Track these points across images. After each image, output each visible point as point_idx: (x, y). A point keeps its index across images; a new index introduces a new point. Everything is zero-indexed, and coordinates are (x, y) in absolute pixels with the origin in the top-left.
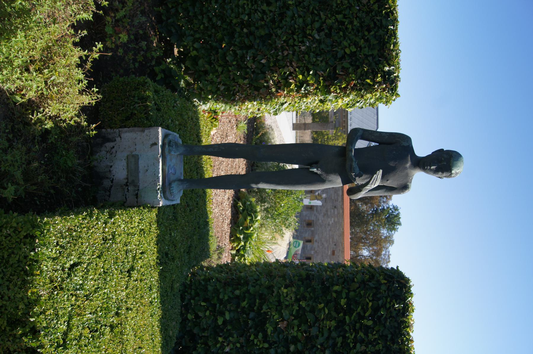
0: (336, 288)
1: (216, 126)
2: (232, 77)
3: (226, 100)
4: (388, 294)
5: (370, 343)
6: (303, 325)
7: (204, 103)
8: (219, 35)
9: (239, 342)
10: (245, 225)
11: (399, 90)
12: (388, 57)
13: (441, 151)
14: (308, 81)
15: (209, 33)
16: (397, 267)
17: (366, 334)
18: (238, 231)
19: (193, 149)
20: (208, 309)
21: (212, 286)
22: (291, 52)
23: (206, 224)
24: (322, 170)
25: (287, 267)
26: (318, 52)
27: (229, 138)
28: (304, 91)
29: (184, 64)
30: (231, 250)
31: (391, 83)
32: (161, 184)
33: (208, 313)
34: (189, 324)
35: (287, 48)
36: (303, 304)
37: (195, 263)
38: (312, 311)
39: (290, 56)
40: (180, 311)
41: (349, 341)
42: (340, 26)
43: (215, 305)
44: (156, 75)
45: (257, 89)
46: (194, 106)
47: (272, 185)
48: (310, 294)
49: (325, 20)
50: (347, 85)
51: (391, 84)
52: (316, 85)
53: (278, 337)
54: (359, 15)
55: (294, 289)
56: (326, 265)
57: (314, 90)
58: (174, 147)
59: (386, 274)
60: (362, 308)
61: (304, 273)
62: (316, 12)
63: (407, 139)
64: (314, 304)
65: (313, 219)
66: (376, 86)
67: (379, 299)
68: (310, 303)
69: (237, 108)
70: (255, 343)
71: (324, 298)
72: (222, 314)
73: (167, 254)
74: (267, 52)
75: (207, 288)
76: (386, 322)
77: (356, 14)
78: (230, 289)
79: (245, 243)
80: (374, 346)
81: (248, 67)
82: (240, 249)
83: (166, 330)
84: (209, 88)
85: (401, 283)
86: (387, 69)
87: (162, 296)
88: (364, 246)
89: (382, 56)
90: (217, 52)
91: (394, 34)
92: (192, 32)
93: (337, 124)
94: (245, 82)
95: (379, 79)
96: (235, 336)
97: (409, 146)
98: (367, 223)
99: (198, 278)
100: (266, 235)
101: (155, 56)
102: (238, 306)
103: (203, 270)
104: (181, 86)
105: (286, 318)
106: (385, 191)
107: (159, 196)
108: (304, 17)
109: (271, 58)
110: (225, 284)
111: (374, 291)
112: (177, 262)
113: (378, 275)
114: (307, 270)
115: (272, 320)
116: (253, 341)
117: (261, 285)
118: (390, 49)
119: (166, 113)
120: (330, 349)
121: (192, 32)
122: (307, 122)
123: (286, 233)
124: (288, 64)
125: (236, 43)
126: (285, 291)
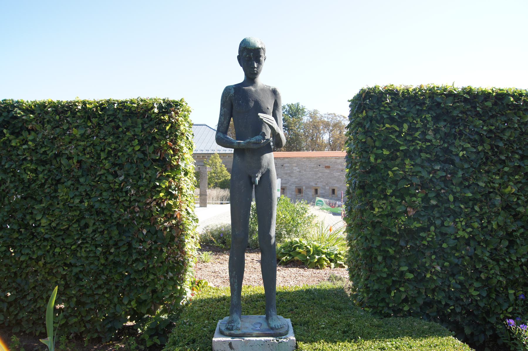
0: (372, 159)
1: (206, 283)
2: (160, 264)
3: (183, 270)
4: (376, 109)
5: (425, 126)
6: (410, 192)
7: (185, 294)
8: (116, 277)
9: (430, 256)
10: (305, 253)
11: (177, 99)
12: (145, 109)
13: (239, 58)
14: (166, 187)
15: (113, 287)
16: (349, 101)
17: (417, 130)
18: (311, 261)
19: (235, 304)
20: (397, 289)
21: (374, 285)
22: (136, 204)
23: (308, 291)
24: (258, 172)
25: (351, 208)
26: (137, 177)
27: (217, 270)
28: (176, 191)
29: (144, 315)
30: (330, 268)
31: (170, 107)
32: (272, 338)
33: (402, 289)
34: (414, 308)
35: (132, 208)
36: (389, 192)
37: (350, 303)
38: (396, 182)
39: (141, 204)
40: (402, 318)
41: (424, 146)
42: (112, 155)
43: (393, 281)
44: (155, 344)
45: (172, 238)
46: (187, 304)
47: (272, 223)
48: (379, 185)
49: (105, 169)
50: (171, 148)
51: (171, 106)
52: (171, 179)
53: (424, 216)
54: (102, 136)
55: (375, 201)
56: (348, 170)
57: (174, 181)
58: (233, 324)
59: (357, 112)
60: (391, 133)
61: (358, 192)
62: (97, 179)
63: (227, 90)
64: (389, 181)
65: (294, 188)
66: (173, 121)
67: (382, 118)
68: (388, 184)
69: (190, 259)
70: (431, 239)
71: (383, 171)
72: (402, 274)
73: (344, 332)
74: (136, 228)
75: (376, 290)
76: (404, 111)
77: (101, 139)
78: (377, 266)
79: (323, 254)
80: (428, 121)
81: (150, 248)
82: (329, 259)
83: (423, 332)
84: (171, 288)
85: (365, 97)
86: (156, 111)
87: (388, 337)
88: (320, 138)
89: (143, 115)
90: (135, 279)
91: (123, 104)
92: (112, 306)
93: (201, 164)
94: (165, 251)
95: (166, 118)
96: (424, 260)
97: (234, 88)
98: (297, 135)
99: (365, 300)
100: (313, 233)
101: (135, 345)
102: (392, 257)
103: (357, 295)
104: (167, 318)
105: (404, 209)
106: (278, 111)
107: (285, 340)
108: (101, 190)
109: (141, 224)
110: (371, 271)
111: (374, 122)
112: (352, 321)
113: (358, 119)
114: (354, 189)
115: (407, 223)
116: (428, 242)
117: (372, 234)
118: (137, 107)
119: (197, 333)
120: (433, 164)
121: (112, 306)
122: (199, 193)
123: (312, 213)
124: (149, 207)
125: (125, 260)
126: (377, 210)
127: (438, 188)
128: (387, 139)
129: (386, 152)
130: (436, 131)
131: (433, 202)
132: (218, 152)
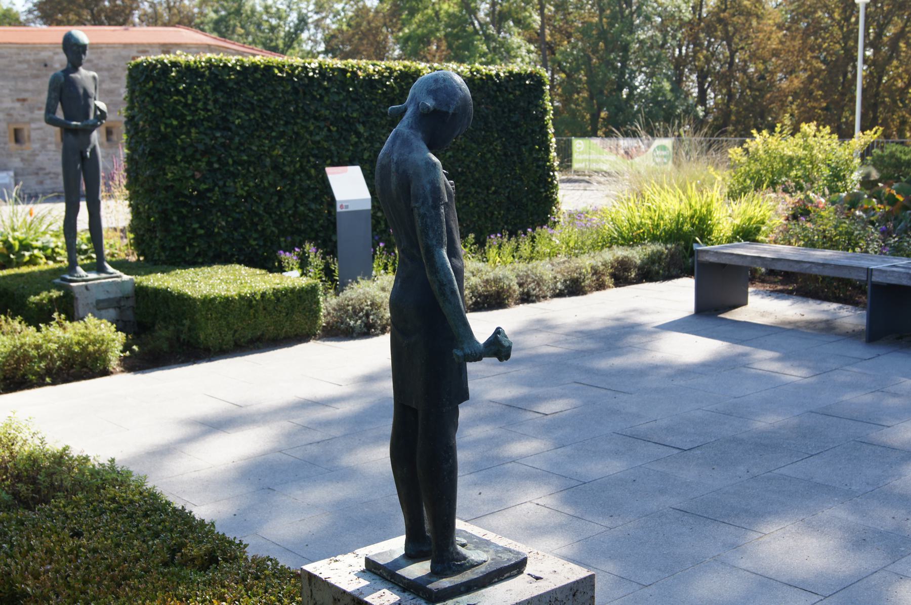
17: (199, 100)
33: (195, 244)
36: (179, 158)
72: (194, 230)
126: (170, 175)
127: (219, 153)
129: (175, 123)
130: (216, 101)
131: (216, 166)
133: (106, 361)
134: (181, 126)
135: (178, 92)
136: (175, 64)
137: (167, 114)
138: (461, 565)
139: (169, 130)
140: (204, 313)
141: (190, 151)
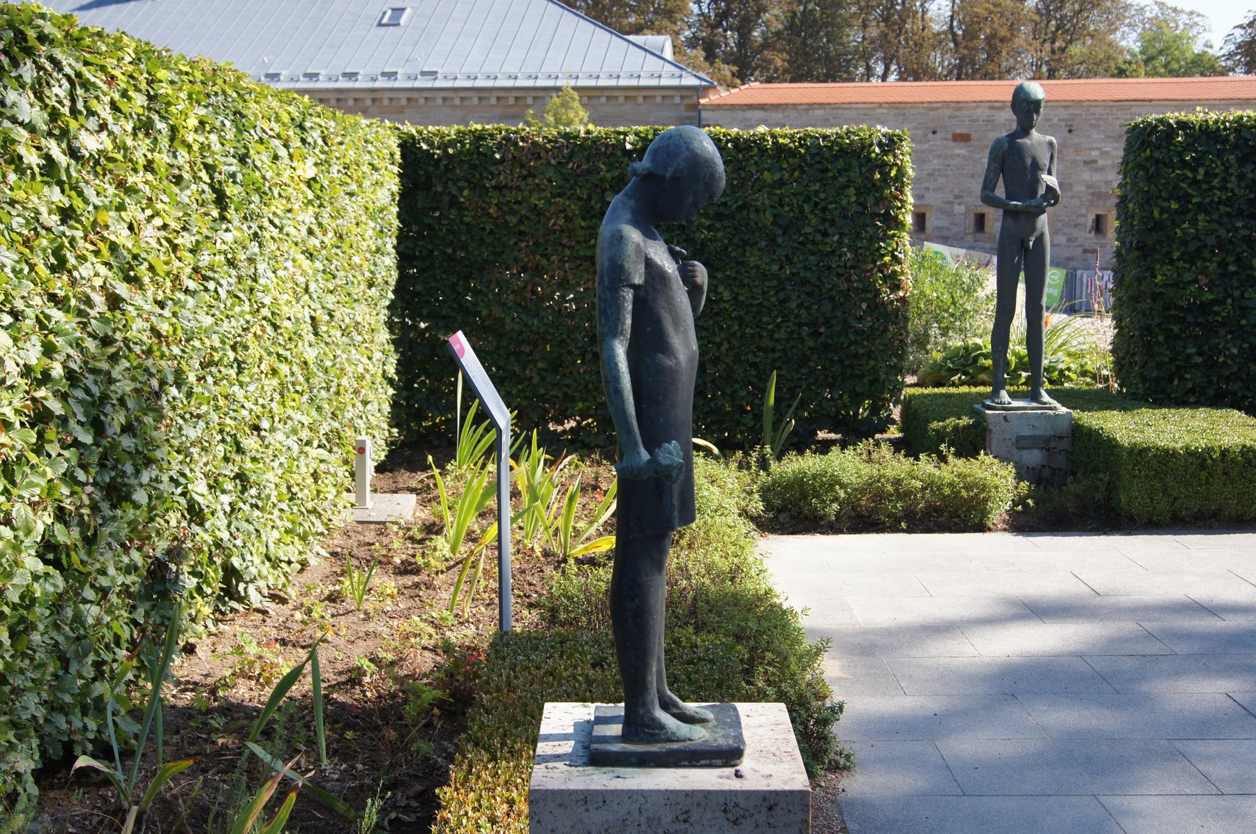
0: (1156, 214)
17: (1216, 176)
33: (1188, 376)
36: (1176, 255)
60: (1183, 181)
72: (1189, 357)
102: (1177, 337)
117: (1151, 309)
126: (1159, 278)
127: (1239, 250)
128: (1176, 187)
129: (1174, 206)
130: (1241, 177)
131: (1232, 268)
132: (572, 83)
133: (984, 513)
134: (1183, 212)
135: (1184, 164)
136: (1183, 125)
137: (1164, 194)
138: (653, 735)
139: (1165, 216)
140: (1129, 467)
141: (1192, 247)
